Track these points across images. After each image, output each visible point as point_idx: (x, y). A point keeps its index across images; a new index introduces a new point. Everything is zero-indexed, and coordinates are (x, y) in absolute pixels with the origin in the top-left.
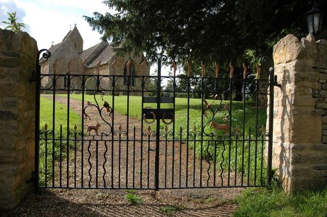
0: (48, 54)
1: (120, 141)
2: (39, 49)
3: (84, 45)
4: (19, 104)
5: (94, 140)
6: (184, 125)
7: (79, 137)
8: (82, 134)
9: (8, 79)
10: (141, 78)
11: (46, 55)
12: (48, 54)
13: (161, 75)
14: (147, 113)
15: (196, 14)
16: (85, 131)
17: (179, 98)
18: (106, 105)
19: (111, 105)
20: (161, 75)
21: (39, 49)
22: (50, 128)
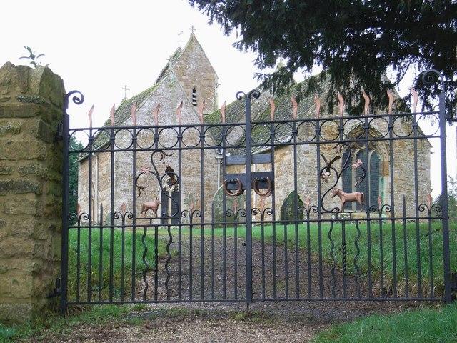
0: (80, 98)
1: (191, 226)
2: (67, 92)
3: (219, 90)
4: (23, 169)
5: (152, 226)
6: (107, 203)
7: (128, 222)
8: (133, 217)
9: (25, 136)
10: (154, 129)
11: (78, 99)
12: (80, 98)
13: (439, 139)
14: (230, 184)
15: (317, 39)
16: (138, 211)
17: (431, 170)
18: (169, 171)
19: (176, 171)
20: (439, 139)
21: (67, 92)
22: (129, 209)
